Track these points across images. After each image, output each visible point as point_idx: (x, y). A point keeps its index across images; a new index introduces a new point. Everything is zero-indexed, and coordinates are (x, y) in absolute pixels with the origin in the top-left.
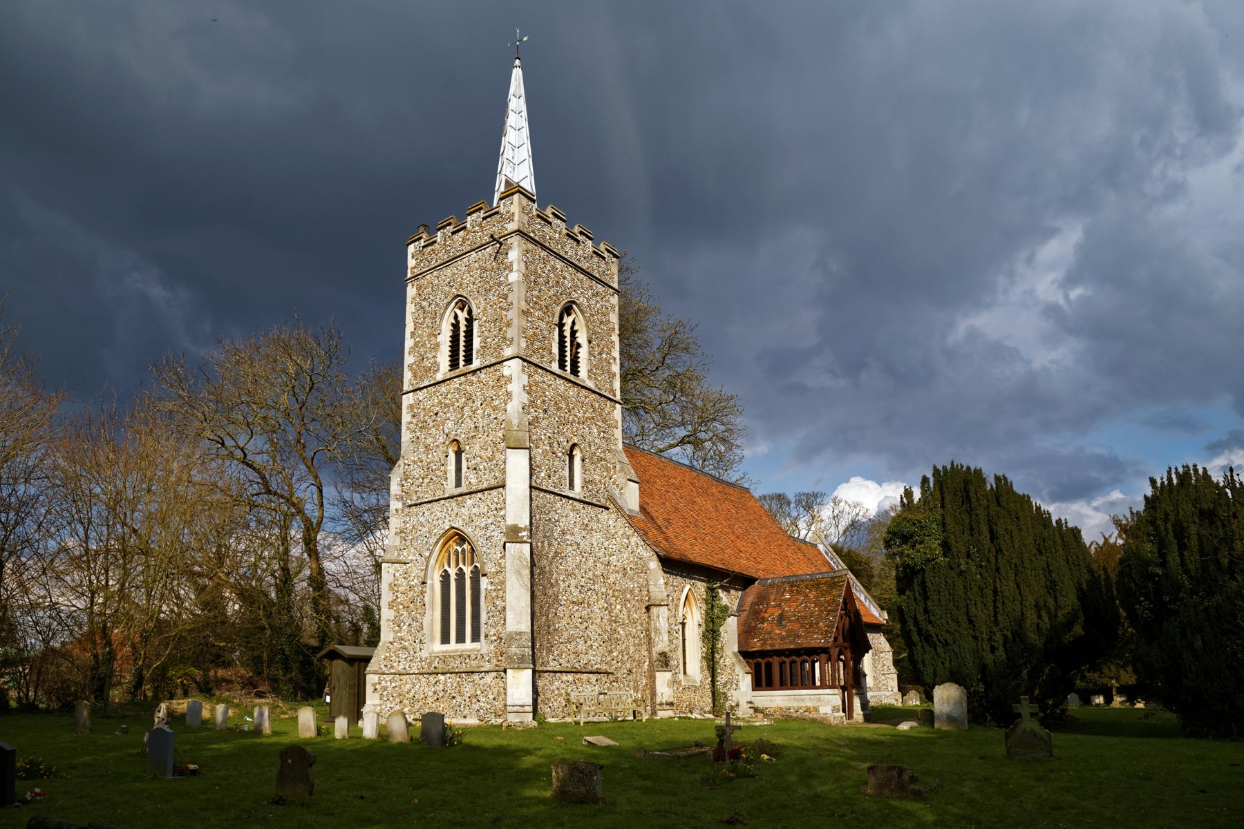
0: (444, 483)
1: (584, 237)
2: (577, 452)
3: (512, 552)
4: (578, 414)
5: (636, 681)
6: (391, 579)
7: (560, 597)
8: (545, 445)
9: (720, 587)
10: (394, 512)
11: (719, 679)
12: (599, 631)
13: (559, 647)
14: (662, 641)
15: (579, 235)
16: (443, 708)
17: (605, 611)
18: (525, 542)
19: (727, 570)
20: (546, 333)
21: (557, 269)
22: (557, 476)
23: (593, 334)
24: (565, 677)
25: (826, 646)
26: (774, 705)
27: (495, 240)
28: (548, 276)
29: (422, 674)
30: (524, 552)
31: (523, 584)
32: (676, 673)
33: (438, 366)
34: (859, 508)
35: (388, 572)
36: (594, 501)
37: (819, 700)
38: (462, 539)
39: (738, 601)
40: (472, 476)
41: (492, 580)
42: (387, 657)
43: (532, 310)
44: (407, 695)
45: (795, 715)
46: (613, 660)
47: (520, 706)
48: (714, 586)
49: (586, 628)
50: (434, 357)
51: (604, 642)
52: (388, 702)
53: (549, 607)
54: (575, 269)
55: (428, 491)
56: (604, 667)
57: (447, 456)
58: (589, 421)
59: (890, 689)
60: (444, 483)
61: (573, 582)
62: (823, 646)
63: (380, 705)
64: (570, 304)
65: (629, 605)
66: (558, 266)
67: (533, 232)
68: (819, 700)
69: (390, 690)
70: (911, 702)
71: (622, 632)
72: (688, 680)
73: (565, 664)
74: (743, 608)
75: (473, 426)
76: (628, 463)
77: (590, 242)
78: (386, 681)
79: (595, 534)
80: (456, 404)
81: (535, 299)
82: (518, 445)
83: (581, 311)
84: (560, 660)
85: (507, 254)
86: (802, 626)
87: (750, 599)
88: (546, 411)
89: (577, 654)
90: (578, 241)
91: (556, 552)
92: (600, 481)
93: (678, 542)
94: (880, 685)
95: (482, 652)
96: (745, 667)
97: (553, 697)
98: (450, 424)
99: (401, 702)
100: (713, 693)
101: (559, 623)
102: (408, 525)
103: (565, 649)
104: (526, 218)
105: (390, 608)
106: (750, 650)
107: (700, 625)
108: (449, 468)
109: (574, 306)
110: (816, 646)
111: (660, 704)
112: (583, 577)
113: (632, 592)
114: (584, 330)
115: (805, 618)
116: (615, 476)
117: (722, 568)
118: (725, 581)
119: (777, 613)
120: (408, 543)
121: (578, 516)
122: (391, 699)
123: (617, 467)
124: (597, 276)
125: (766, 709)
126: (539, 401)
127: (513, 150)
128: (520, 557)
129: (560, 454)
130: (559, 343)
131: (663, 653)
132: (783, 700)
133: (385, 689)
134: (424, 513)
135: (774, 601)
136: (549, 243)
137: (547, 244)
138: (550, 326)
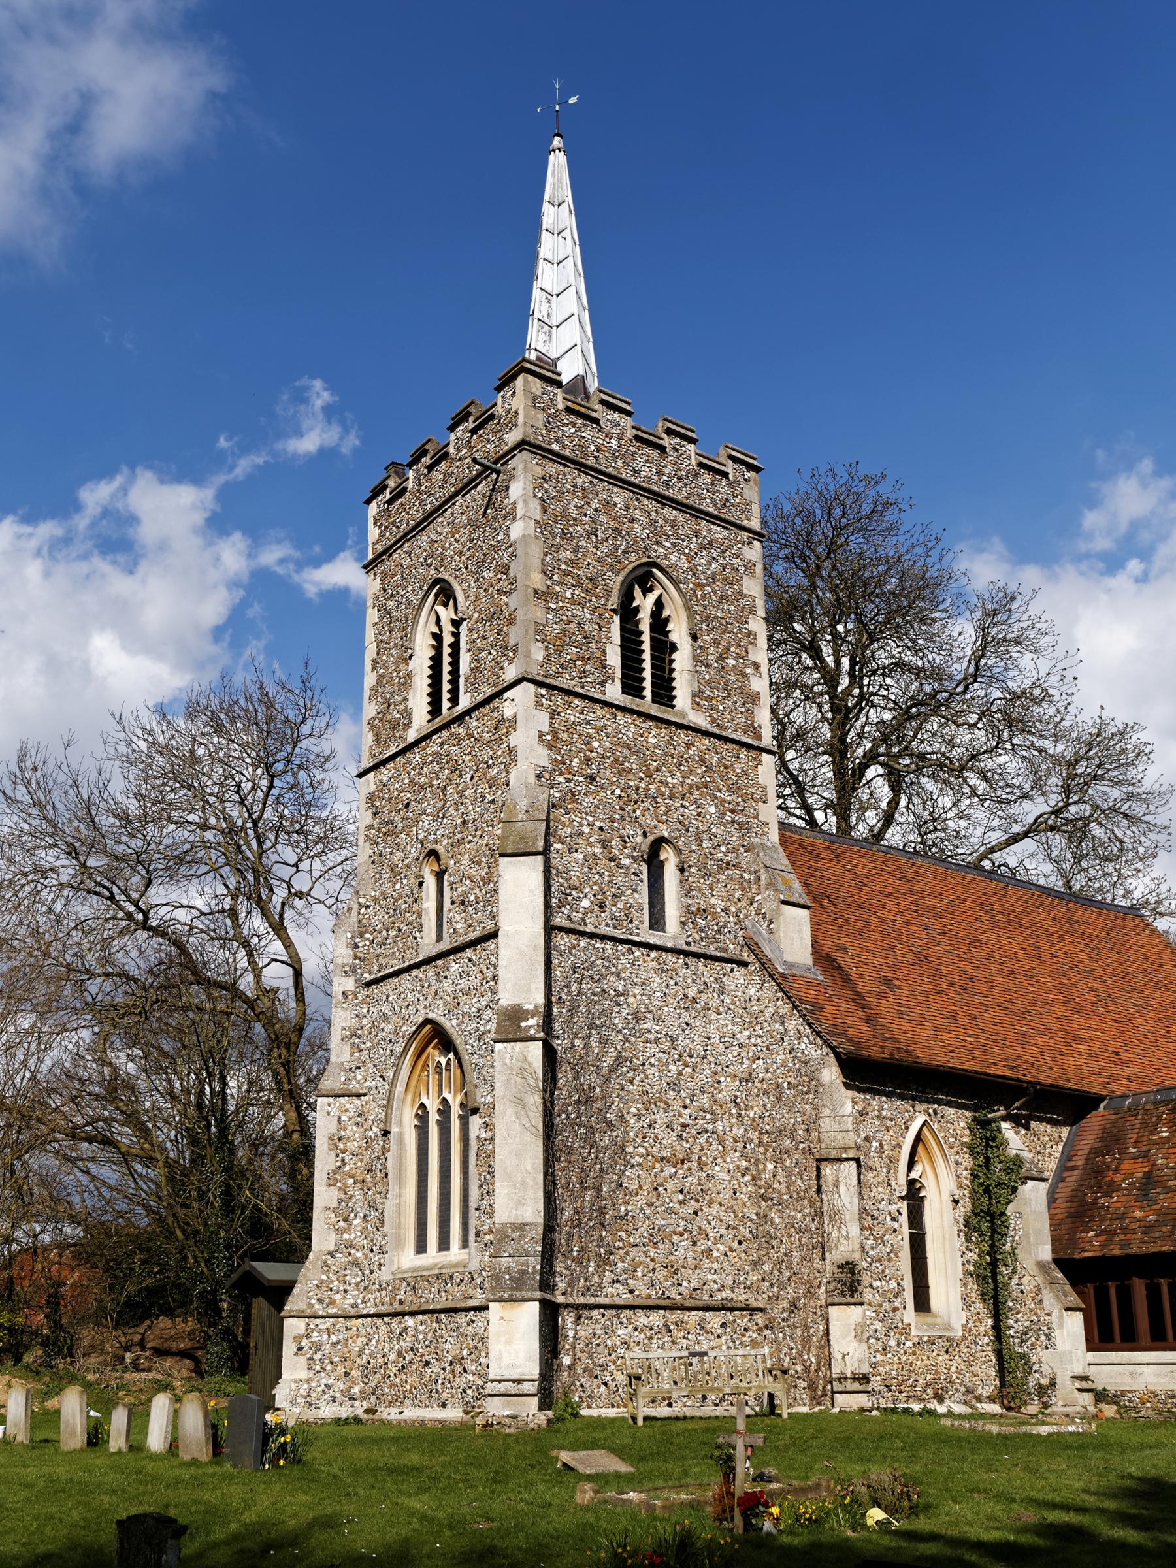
0: (418, 934)
1: (677, 440)
2: (668, 855)
3: (508, 1061)
4: (669, 780)
5: (806, 1327)
6: (333, 1128)
7: (630, 1149)
8: (590, 844)
9: (1005, 1118)
10: (340, 997)
11: (1011, 1322)
12: (729, 1218)
13: (627, 1253)
14: (847, 1238)
15: (665, 436)
16: (411, 1386)
17: (744, 1175)
18: (532, 1039)
19: (1017, 1080)
20: (590, 629)
21: (615, 505)
22: (620, 905)
23: (702, 621)
24: (641, 1319)
26: (1139, 1385)
27: (486, 468)
28: (594, 521)
30: (529, 1059)
31: (527, 1125)
32: (895, 1309)
33: (410, 714)
35: (328, 1114)
36: (712, 950)
38: (447, 1045)
39: (1060, 1148)
40: (458, 917)
41: (487, 1119)
42: (322, 1282)
43: (557, 588)
44: (358, 1360)
46: (763, 1280)
47: (514, 1381)
48: (990, 1116)
49: (696, 1213)
50: (405, 699)
51: (740, 1243)
52: (323, 1374)
53: (601, 1170)
54: (658, 502)
55: (393, 953)
56: (741, 1296)
57: (421, 884)
58: (695, 792)
60: (418, 934)
61: (661, 1118)
63: (308, 1381)
64: (646, 569)
65: (788, 1163)
66: (618, 500)
67: (558, 441)
69: (327, 1348)
71: (777, 1221)
72: (931, 1326)
73: (641, 1289)
75: (459, 821)
76: (789, 868)
77: (692, 447)
78: (320, 1331)
79: (714, 1016)
80: (435, 782)
81: (564, 567)
82: (521, 848)
83: (675, 582)
84: (630, 1282)
85: (507, 489)
87: (1088, 1142)
88: (592, 778)
89: (673, 1269)
90: (662, 449)
91: (619, 1057)
92: (726, 910)
93: (897, 1025)
95: (470, 1269)
96: (1065, 1295)
97: (614, 1363)
98: (426, 821)
99: (347, 1374)
100: (999, 1354)
101: (626, 1203)
102: (365, 1022)
103: (643, 1259)
104: (541, 416)
105: (330, 1185)
106: (1077, 1256)
107: (956, 1202)
108: (426, 905)
109: (655, 571)
111: (839, 1379)
112: (685, 1107)
113: (792, 1135)
114: (683, 615)
116: (759, 897)
117: (1003, 1077)
118: (1017, 1104)
119: (1141, 1170)
120: (365, 1056)
121: (672, 982)
122: (329, 1368)
123: (763, 877)
124: (711, 509)
125: (1123, 1393)
126: (576, 760)
127: (549, 301)
128: (523, 1069)
129: (627, 862)
130: (621, 646)
131: (847, 1263)
132: (1158, 1375)
133: (317, 1347)
134: (388, 996)
135: (1136, 1144)
136: (596, 457)
137: (591, 461)
138: (601, 615)
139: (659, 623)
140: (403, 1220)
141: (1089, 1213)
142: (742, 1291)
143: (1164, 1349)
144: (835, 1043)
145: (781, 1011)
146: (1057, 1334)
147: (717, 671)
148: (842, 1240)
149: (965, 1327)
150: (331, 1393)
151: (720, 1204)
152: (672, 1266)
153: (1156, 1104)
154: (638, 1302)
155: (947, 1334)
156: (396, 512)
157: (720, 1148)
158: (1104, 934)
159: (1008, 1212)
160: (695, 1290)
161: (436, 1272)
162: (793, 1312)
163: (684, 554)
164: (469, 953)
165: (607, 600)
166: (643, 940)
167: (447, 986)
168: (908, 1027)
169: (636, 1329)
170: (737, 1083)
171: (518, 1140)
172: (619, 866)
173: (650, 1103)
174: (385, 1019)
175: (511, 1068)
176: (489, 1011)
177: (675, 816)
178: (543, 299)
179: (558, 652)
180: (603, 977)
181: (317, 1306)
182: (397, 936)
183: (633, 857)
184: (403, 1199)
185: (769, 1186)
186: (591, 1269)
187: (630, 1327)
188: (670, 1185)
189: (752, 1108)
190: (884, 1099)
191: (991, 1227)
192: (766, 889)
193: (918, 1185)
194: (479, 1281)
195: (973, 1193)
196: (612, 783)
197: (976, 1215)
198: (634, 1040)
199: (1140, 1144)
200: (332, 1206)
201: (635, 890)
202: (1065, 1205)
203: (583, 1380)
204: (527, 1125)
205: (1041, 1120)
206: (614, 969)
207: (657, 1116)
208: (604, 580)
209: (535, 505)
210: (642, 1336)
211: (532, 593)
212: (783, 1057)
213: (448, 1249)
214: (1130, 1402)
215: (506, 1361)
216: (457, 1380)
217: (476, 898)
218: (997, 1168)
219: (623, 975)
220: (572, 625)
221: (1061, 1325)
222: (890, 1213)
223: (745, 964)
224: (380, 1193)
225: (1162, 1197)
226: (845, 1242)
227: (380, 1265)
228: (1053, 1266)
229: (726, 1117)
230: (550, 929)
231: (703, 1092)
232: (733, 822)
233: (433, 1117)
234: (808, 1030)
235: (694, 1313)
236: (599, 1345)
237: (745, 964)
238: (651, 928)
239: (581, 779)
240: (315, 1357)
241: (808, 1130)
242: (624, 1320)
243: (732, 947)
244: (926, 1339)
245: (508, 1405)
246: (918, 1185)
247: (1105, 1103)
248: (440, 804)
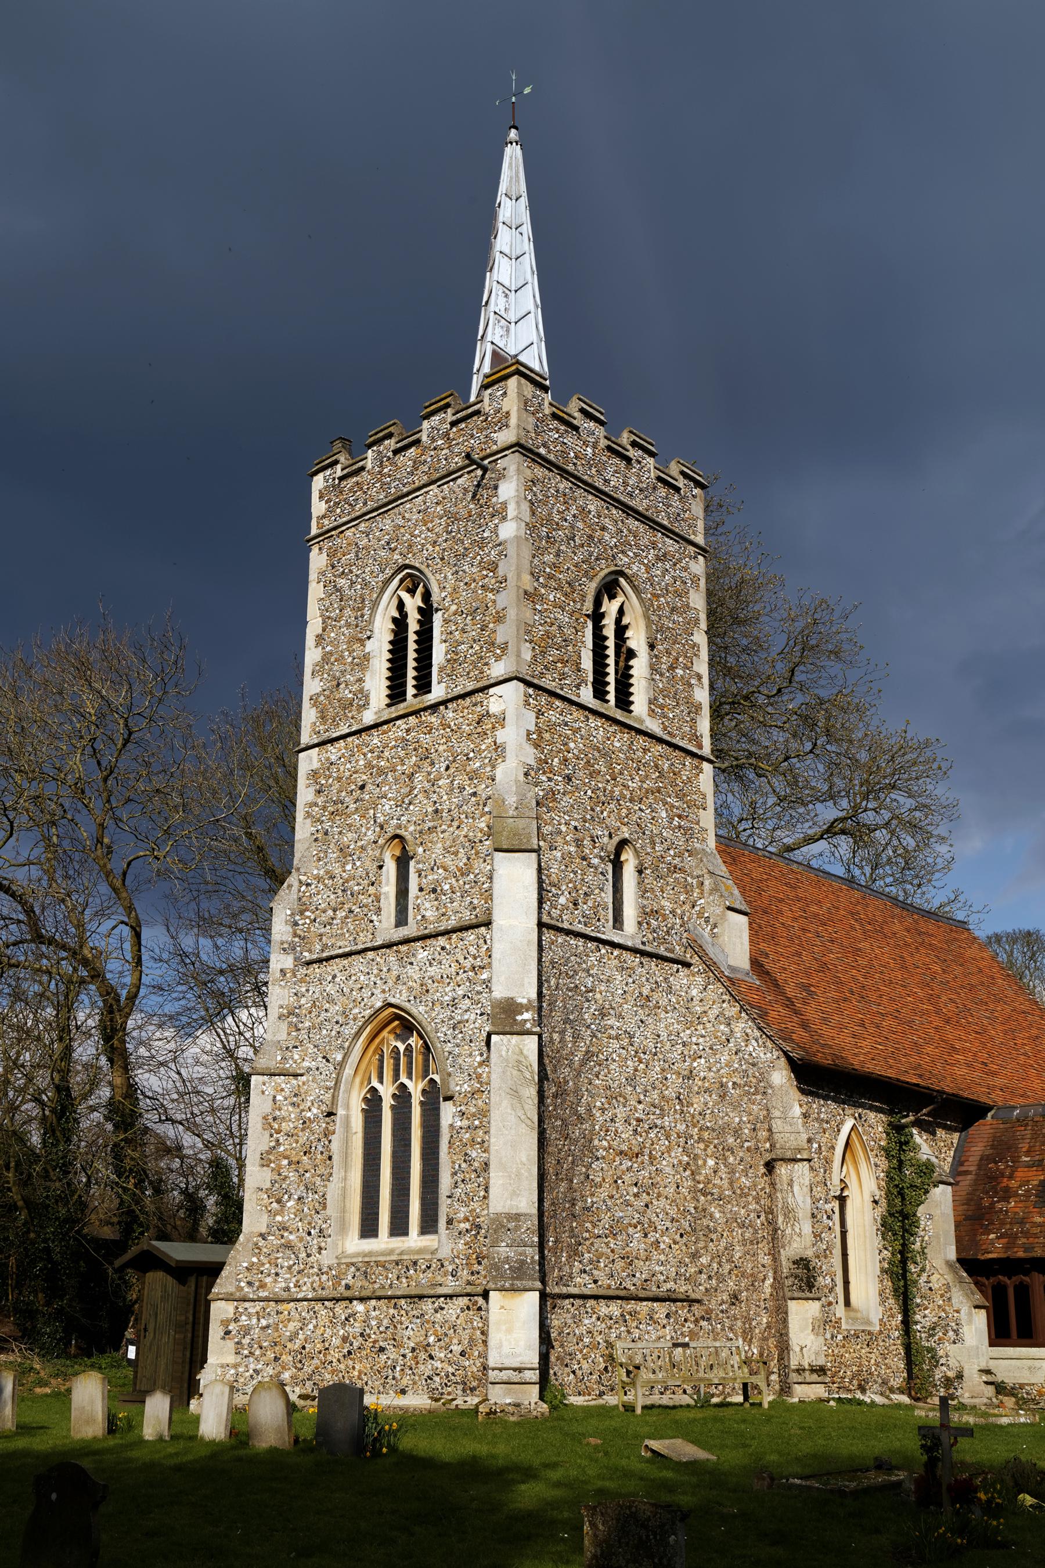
0: (374, 918)
1: (640, 452)
3: (504, 1053)
4: (630, 783)
5: (748, 1319)
6: (267, 1107)
7: (596, 1142)
8: (566, 843)
10: (278, 975)
12: (673, 1212)
13: (592, 1244)
14: (800, 1235)
15: (629, 447)
16: (360, 1372)
17: (685, 1170)
18: (529, 1033)
19: (928, 1088)
21: (590, 512)
22: (590, 903)
23: (657, 631)
24: (604, 1309)
28: (572, 527)
29: (322, 1300)
30: (525, 1052)
31: (523, 1117)
33: (367, 697)
35: (263, 1092)
36: (662, 951)
40: (427, 905)
41: (463, 1108)
42: (253, 1263)
43: (543, 591)
44: (289, 1345)
46: (701, 1272)
47: (515, 1370)
49: (647, 1206)
50: (360, 680)
51: (682, 1236)
52: (251, 1359)
53: (573, 1162)
54: (624, 512)
55: (343, 934)
56: (683, 1288)
57: (381, 867)
58: (651, 797)
60: (374, 918)
61: (621, 1112)
63: (236, 1366)
64: (613, 577)
65: (731, 1160)
66: (592, 508)
67: (545, 445)
71: (717, 1215)
73: (604, 1281)
75: (430, 810)
76: (727, 875)
77: (651, 460)
78: (249, 1316)
80: (399, 768)
81: (548, 570)
84: (595, 1272)
85: (496, 487)
87: (978, 1149)
88: (568, 779)
90: (628, 460)
91: (587, 1052)
93: (827, 1031)
95: (439, 1256)
97: (581, 1351)
98: (387, 806)
99: (276, 1359)
100: (908, 1348)
102: (303, 1001)
103: (605, 1250)
104: (532, 420)
107: (875, 1202)
108: (385, 889)
109: (622, 580)
111: (798, 1371)
112: (640, 1102)
113: (737, 1133)
114: (642, 624)
116: (702, 901)
117: (917, 1085)
121: (630, 980)
122: (258, 1352)
123: (707, 883)
124: (665, 523)
125: (1022, 1386)
127: (506, 296)
128: (519, 1062)
129: (596, 861)
130: (593, 650)
131: (801, 1259)
133: (246, 1331)
134: (334, 977)
135: (1028, 1153)
136: (575, 464)
137: (570, 468)
139: (621, 630)
140: (347, 1205)
142: (683, 1282)
144: (788, 1048)
145: (727, 1014)
147: (669, 680)
148: (795, 1237)
150: (260, 1378)
151: (667, 1198)
152: (628, 1258)
154: (601, 1292)
155: (868, 1328)
156: (350, 490)
157: (667, 1143)
158: (945, 947)
160: (646, 1281)
161: (394, 1257)
162: (733, 1304)
163: (644, 564)
164: (442, 941)
165: (582, 605)
166: (609, 938)
167: (412, 972)
168: (833, 1033)
169: (598, 1319)
170: (681, 1080)
171: (513, 1132)
172: (589, 865)
173: (613, 1097)
174: (331, 1000)
175: (507, 1060)
176: (467, 1001)
177: (634, 819)
178: (500, 293)
179: (543, 653)
180: (576, 972)
181: (246, 1289)
182: (346, 917)
183: (601, 857)
184: (348, 1182)
185: (709, 1182)
186: (563, 1259)
187: (594, 1316)
188: (626, 1178)
189: (692, 1105)
191: (903, 1227)
192: (710, 894)
194: (450, 1269)
195: (888, 1194)
196: (585, 784)
198: (599, 1035)
199: (1033, 1154)
200: (265, 1187)
201: (602, 890)
203: (556, 1368)
204: (523, 1117)
206: (584, 966)
207: (617, 1111)
208: (580, 585)
209: (525, 507)
210: (604, 1325)
211: (521, 591)
212: (728, 1058)
213: (376, 1234)
214: (1027, 1394)
215: (506, 1350)
216: (422, 1367)
217: (451, 887)
219: (591, 972)
220: (554, 628)
223: (687, 965)
224: (321, 1176)
226: (798, 1239)
227: (320, 1248)
228: (957, 1265)
229: (672, 1112)
230: (541, 925)
231: (654, 1088)
232: (680, 827)
233: (387, 1102)
234: (757, 1033)
235: (645, 1303)
236: (568, 1334)
237: (687, 965)
238: (614, 928)
239: (560, 779)
240: (244, 1341)
241: (754, 1129)
242: (589, 1310)
243: (677, 948)
244: (852, 1332)
245: (508, 1393)
247: (993, 1112)
248: (405, 790)
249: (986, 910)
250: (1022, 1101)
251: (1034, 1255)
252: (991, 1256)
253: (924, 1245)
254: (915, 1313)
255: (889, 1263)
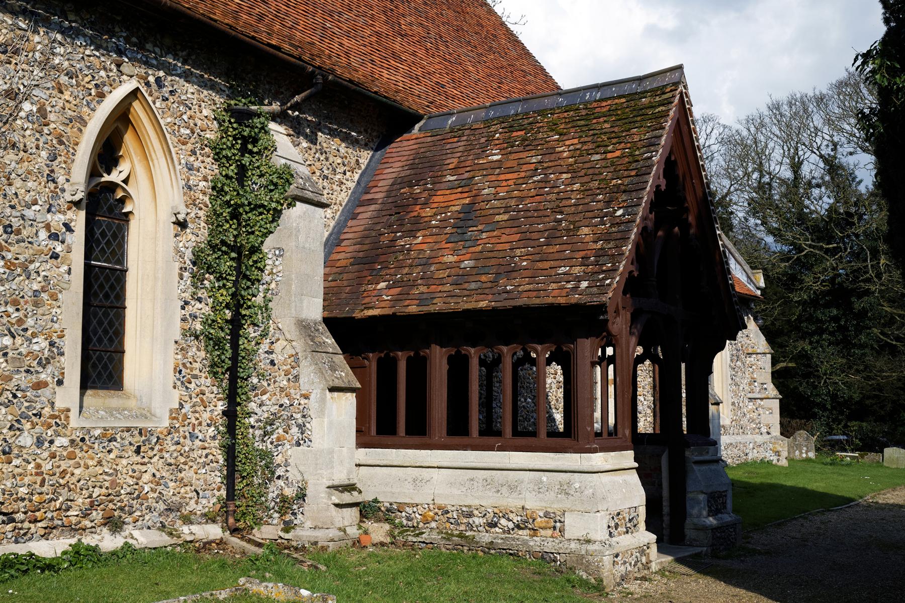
9: (274, 117)
11: (252, 406)
25: (596, 300)
26: (423, 497)
32: (39, 385)
34: (711, 124)
37: (564, 490)
39: (356, 177)
45: (485, 538)
48: (253, 108)
59: (764, 430)
62: (584, 299)
68: (564, 490)
70: (797, 453)
74: (369, 196)
86: (526, 240)
94: (744, 422)
96: (333, 369)
100: (230, 453)
106: (358, 315)
110: (562, 301)
115: (539, 213)
119: (458, 202)
125: (401, 507)
141: (382, 258)
143: (464, 448)
146: (315, 427)
149: (175, 414)
153: (488, 122)
159: (265, 249)
190: (59, 37)
191: (238, 269)
193: (120, 194)
197: (214, 247)
202: (351, 249)
205: (333, 134)
214: (409, 519)
218: (255, 183)
221: (321, 412)
222: (48, 227)
225: (484, 235)
228: (322, 327)
246: (120, 194)
249: (522, 22)
250: (458, 106)
251: (432, 309)
252: (371, 313)
253: (269, 296)
254: (248, 399)
255: (204, 323)
